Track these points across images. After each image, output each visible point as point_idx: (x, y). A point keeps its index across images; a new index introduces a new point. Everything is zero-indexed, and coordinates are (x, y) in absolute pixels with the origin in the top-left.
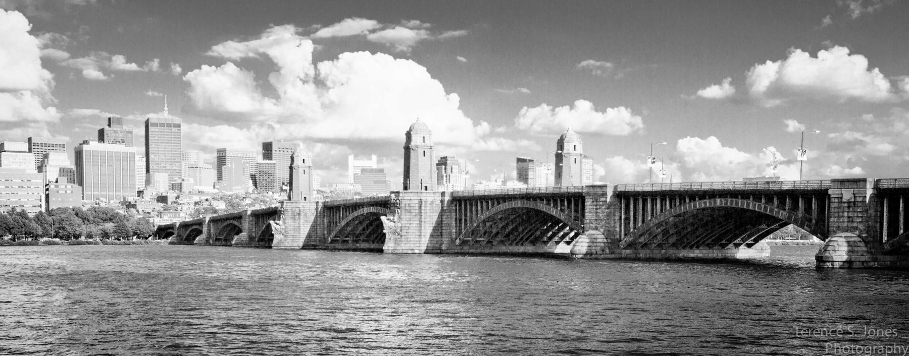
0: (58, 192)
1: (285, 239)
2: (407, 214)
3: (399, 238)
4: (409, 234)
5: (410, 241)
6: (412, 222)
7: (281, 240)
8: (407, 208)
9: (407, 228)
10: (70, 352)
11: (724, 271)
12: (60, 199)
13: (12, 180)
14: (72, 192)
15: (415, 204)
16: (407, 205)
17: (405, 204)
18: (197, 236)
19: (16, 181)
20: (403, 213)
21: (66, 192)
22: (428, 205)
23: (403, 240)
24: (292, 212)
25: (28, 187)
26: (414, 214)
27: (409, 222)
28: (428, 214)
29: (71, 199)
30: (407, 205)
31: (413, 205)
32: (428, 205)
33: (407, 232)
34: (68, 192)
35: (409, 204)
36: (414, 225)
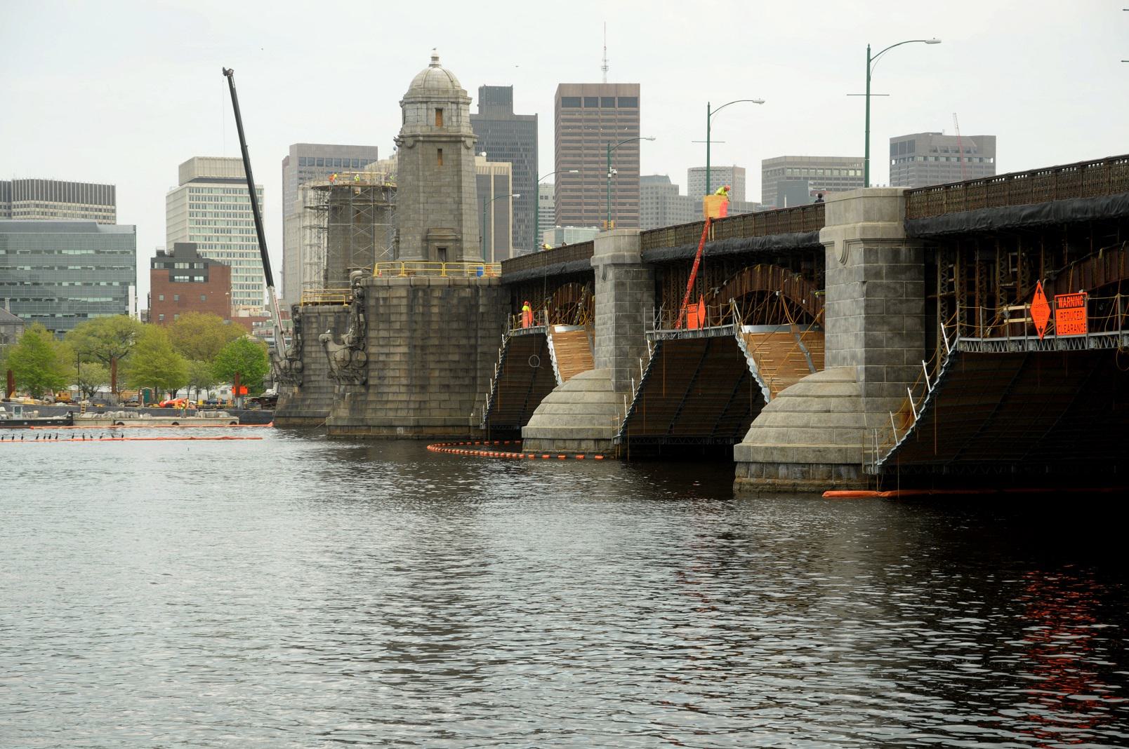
0: (172, 279)
1: (302, 396)
2: (381, 326)
3: (362, 394)
4: (386, 382)
5: (387, 402)
6: (392, 350)
7: (293, 400)
8: (381, 310)
9: (381, 366)
10: (783, 658)
11: (619, 469)
12: (176, 298)
13: (60, 252)
14: (206, 279)
15: (400, 298)
16: (381, 302)
17: (377, 299)
18: (655, 355)
19: (71, 252)
20: (372, 325)
21: (192, 279)
22: (435, 302)
23: (371, 398)
24: (319, 324)
25: (98, 268)
26: (397, 326)
27: (385, 350)
28: (434, 326)
29: (203, 298)
30: (381, 302)
31: (395, 302)
32: (435, 302)
33: (380, 378)
34: (196, 278)
35: (385, 299)
36: (397, 358)
